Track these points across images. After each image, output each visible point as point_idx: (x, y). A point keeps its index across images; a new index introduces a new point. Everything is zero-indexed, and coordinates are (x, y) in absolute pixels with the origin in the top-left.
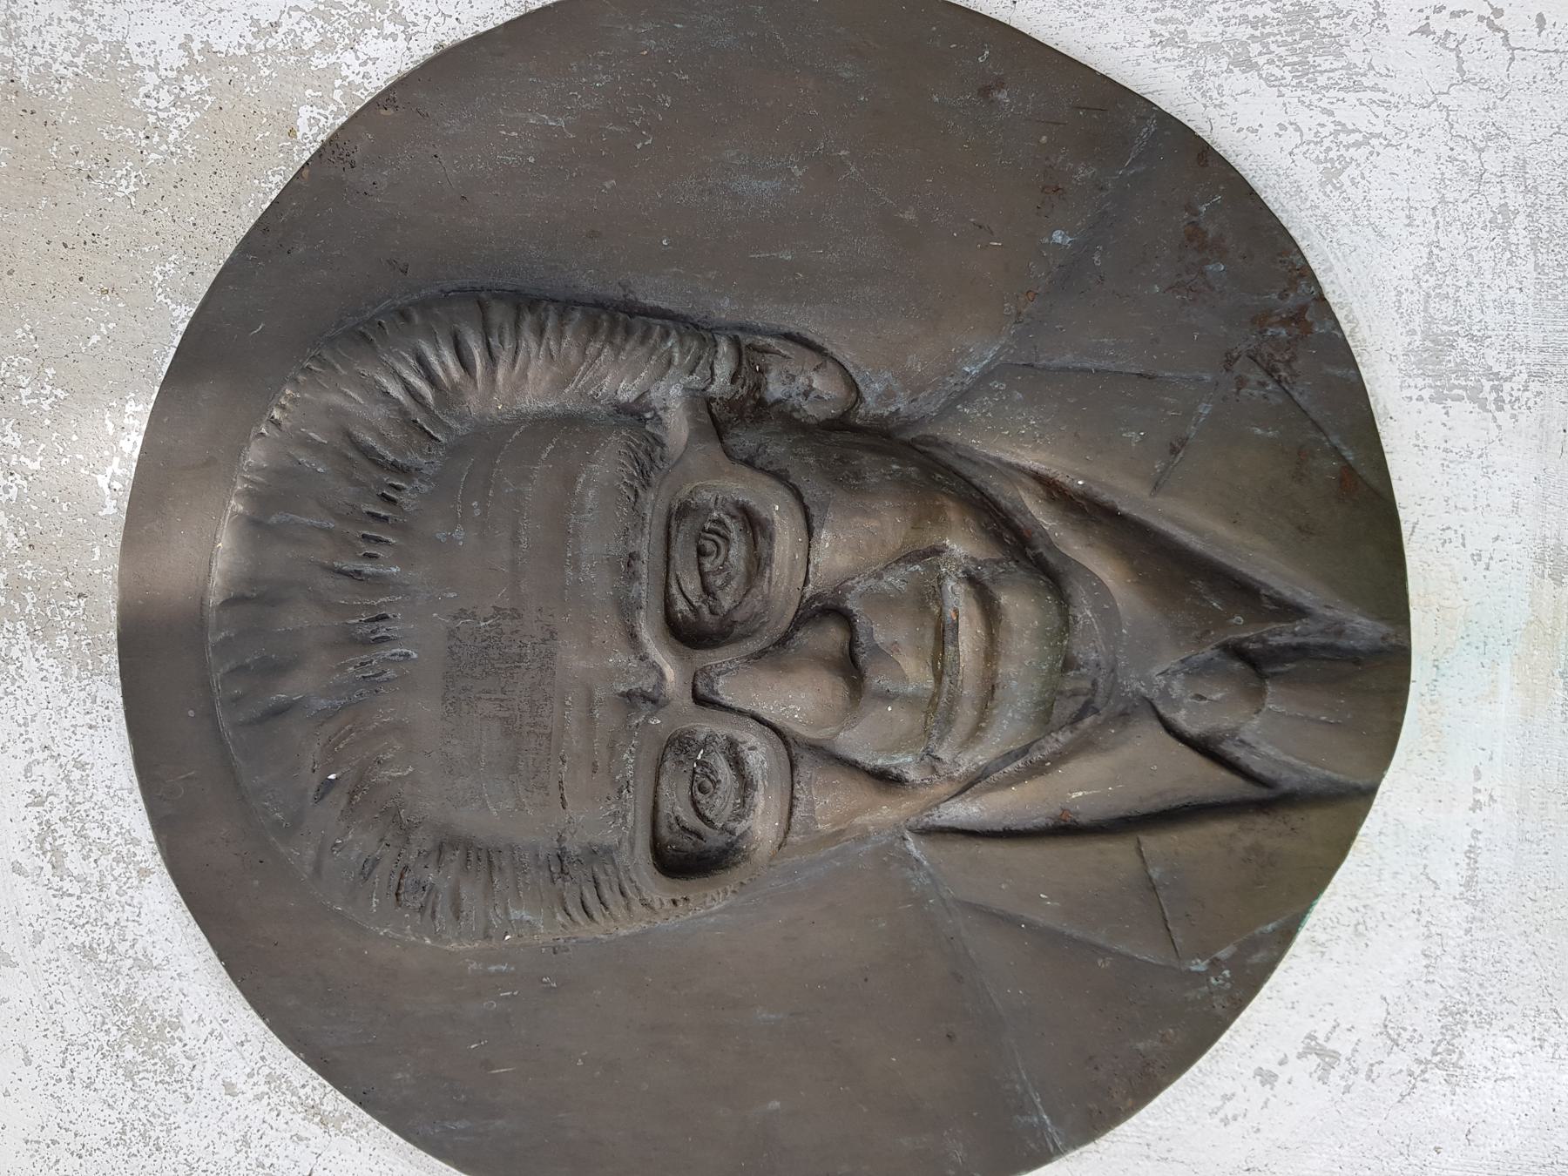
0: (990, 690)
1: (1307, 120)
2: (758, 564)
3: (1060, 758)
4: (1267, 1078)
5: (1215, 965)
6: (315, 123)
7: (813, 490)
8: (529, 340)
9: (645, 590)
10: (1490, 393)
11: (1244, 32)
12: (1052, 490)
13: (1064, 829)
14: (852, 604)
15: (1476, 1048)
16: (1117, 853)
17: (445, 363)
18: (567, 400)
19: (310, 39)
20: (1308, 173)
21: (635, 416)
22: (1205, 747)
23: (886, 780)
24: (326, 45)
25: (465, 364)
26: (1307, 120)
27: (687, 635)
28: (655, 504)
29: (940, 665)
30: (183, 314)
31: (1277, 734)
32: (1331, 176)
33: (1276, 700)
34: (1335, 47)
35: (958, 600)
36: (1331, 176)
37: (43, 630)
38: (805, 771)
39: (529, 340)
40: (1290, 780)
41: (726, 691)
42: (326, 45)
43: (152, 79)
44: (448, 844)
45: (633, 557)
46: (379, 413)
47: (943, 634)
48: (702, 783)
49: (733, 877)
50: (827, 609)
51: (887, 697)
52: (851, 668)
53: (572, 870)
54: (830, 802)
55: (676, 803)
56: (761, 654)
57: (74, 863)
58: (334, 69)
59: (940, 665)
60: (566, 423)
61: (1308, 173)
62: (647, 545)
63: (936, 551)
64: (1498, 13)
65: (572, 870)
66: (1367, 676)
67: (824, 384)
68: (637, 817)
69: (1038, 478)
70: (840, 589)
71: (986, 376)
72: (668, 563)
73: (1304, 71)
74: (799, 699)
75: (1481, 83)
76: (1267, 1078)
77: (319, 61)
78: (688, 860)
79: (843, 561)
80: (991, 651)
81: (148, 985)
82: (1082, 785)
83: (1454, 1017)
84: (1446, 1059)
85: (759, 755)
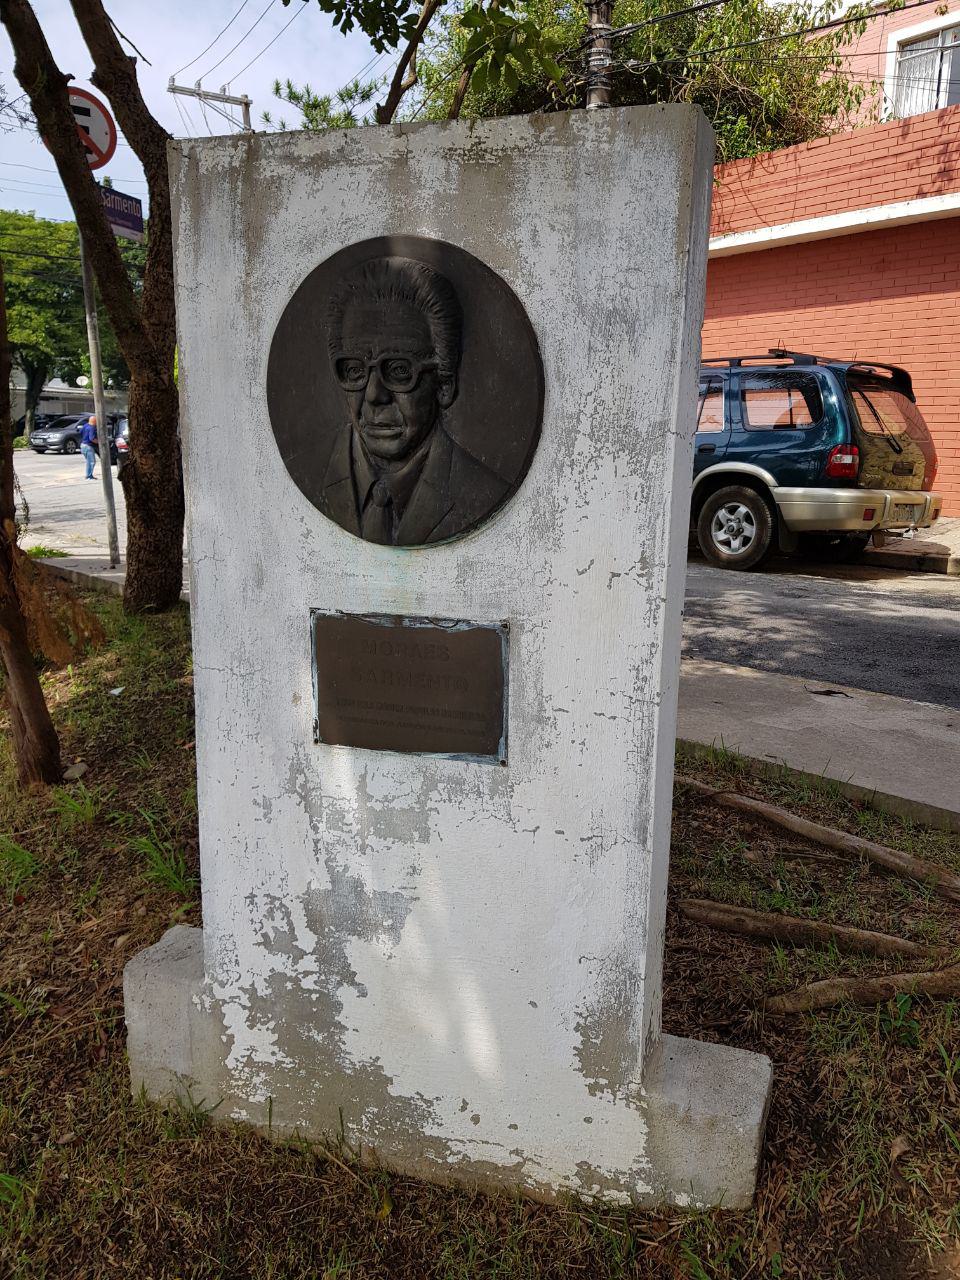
0: (377, 437)
1: (523, 528)
2: (400, 381)
4: (302, 519)
5: (324, 498)
6: (505, 274)
7: (417, 393)
8: (443, 327)
9: (392, 354)
10: (461, 580)
11: (542, 512)
12: (426, 456)
13: (352, 461)
14: (394, 404)
15: (309, 576)
16: (347, 473)
17: (436, 308)
18: (433, 336)
19: (525, 271)
20: (509, 530)
21: (431, 352)
23: (359, 414)
25: (436, 313)
26: (523, 528)
27: (384, 364)
28: (409, 356)
29: (382, 425)
30: (461, 245)
31: (373, 511)
33: (379, 510)
35: (397, 430)
37: (392, 217)
38: (359, 394)
39: (443, 327)
40: (364, 517)
43: (513, 233)
44: (342, 313)
45: (398, 351)
47: (388, 426)
48: (355, 369)
49: (335, 377)
50: (391, 399)
51: (374, 412)
52: (376, 403)
53: (338, 343)
54: (353, 399)
55: (352, 364)
56: (379, 380)
57: (344, 226)
58: (518, 277)
59: (382, 425)
60: (428, 336)
61: (509, 530)
62: (400, 355)
63: (407, 425)
64: (551, 583)
65: (338, 343)
66: (385, 536)
67: (446, 400)
68: (348, 355)
69: (428, 453)
70: (396, 401)
71: (452, 441)
72: (876, 415)
74: (371, 392)
77: (520, 274)
78: (341, 367)
79: (401, 401)
82: (362, 466)
83: (316, 570)
84: (306, 569)
85: (361, 382)
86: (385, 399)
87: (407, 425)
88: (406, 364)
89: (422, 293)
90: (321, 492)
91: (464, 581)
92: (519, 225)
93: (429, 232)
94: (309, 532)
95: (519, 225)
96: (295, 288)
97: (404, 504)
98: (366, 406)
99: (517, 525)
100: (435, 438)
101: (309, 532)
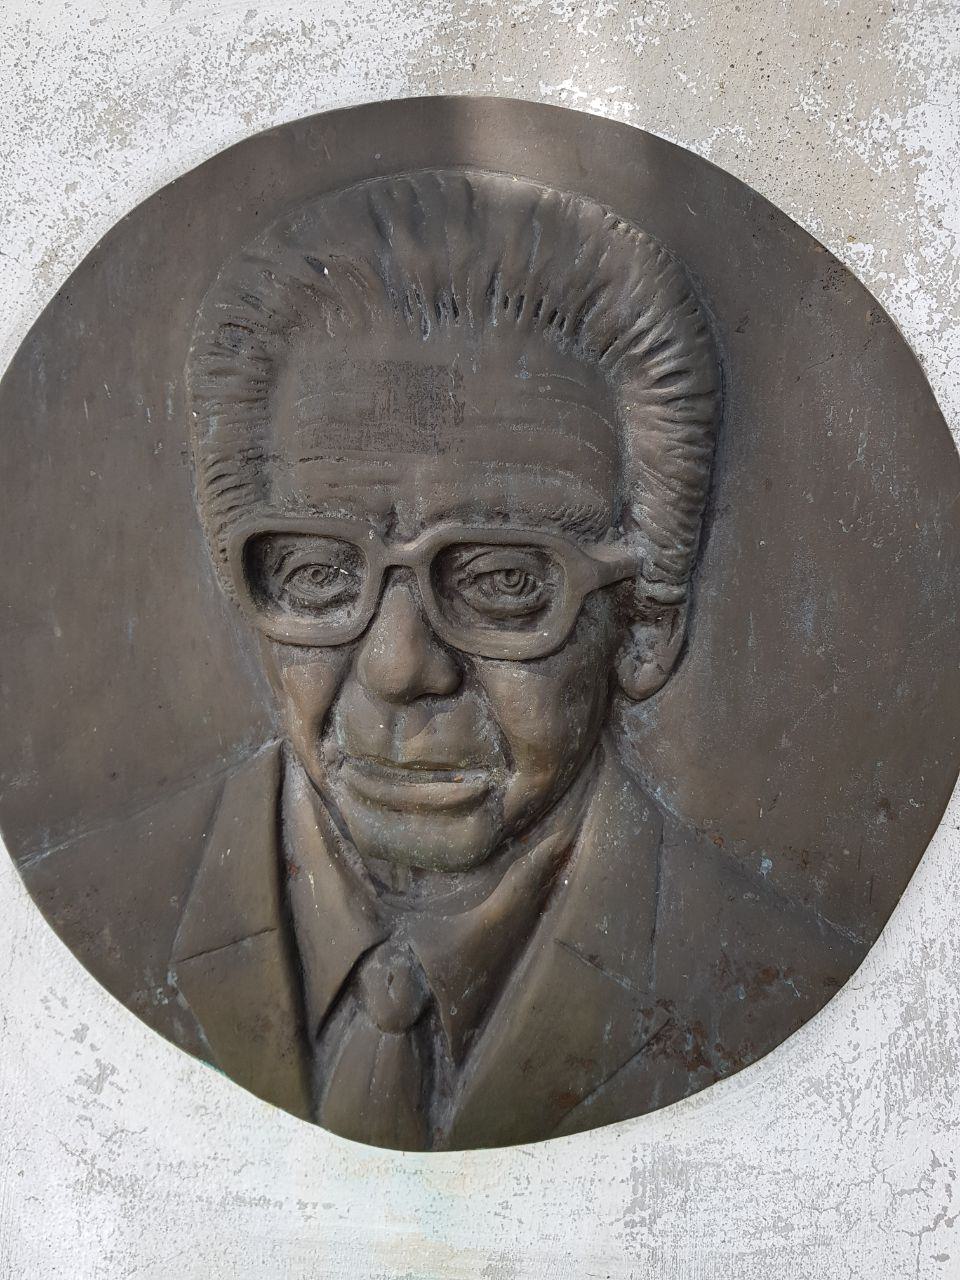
1: (863, 1067)
3: (342, 866)
4: (80, 1034)
6: (860, 257)
7: (560, 663)
8: (682, 431)
9: (479, 527)
11: (933, 1015)
12: (560, 859)
13: (283, 869)
14: (467, 696)
15: (104, 1205)
16: (264, 912)
18: (633, 463)
19: (928, 253)
20: (819, 1068)
22: (350, 984)
24: (923, 266)
25: (662, 380)
27: (442, 560)
28: (548, 535)
29: (419, 767)
31: (361, 1040)
32: (817, 1086)
33: (390, 1041)
34: (922, 1090)
35: (471, 782)
36: (817, 1086)
37: (445, 35)
38: (331, 657)
39: (682, 431)
40: (323, 1053)
41: (396, 593)
42: (923, 266)
43: (896, 124)
45: (506, 517)
46: (623, 310)
47: (443, 770)
48: (320, 572)
49: (243, 596)
50: (463, 675)
51: (391, 724)
53: (248, 470)
54: (306, 677)
55: (305, 552)
57: (256, 60)
58: (904, 272)
59: (419, 767)
61: (819, 1068)
62: (514, 528)
63: (510, 764)
64: (950, 1223)
65: (248, 470)
66: (407, 1118)
70: (480, 686)
71: (653, 805)
73: (902, 1064)
74: (390, 652)
75: (892, 1209)
76: (80, 1034)
77: (910, 261)
78: (258, 561)
80: (428, 809)
81: (155, 121)
82: (320, 885)
84: (96, 1180)
85: (344, 620)
86: (441, 680)
87: (510, 764)
88: (531, 561)
89: (615, 304)
90: (162, 979)
91: (655, 1217)
92: (922, 96)
93: (601, 95)
94: (105, 1071)
95: (922, 96)
96: (61, 273)
97: (478, 1014)
98: (355, 702)
99: (848, 1054)
100: (598, 797)
101: (105, 1071)
